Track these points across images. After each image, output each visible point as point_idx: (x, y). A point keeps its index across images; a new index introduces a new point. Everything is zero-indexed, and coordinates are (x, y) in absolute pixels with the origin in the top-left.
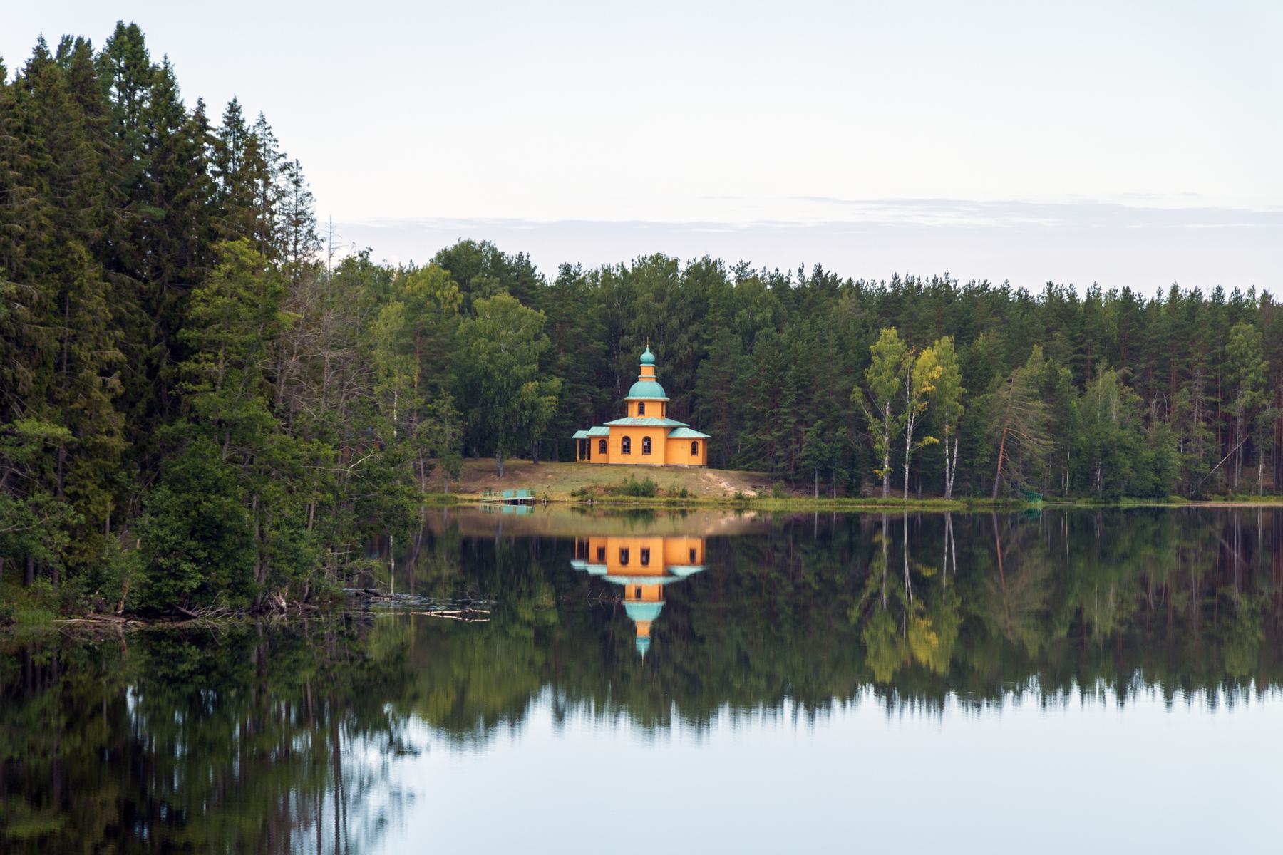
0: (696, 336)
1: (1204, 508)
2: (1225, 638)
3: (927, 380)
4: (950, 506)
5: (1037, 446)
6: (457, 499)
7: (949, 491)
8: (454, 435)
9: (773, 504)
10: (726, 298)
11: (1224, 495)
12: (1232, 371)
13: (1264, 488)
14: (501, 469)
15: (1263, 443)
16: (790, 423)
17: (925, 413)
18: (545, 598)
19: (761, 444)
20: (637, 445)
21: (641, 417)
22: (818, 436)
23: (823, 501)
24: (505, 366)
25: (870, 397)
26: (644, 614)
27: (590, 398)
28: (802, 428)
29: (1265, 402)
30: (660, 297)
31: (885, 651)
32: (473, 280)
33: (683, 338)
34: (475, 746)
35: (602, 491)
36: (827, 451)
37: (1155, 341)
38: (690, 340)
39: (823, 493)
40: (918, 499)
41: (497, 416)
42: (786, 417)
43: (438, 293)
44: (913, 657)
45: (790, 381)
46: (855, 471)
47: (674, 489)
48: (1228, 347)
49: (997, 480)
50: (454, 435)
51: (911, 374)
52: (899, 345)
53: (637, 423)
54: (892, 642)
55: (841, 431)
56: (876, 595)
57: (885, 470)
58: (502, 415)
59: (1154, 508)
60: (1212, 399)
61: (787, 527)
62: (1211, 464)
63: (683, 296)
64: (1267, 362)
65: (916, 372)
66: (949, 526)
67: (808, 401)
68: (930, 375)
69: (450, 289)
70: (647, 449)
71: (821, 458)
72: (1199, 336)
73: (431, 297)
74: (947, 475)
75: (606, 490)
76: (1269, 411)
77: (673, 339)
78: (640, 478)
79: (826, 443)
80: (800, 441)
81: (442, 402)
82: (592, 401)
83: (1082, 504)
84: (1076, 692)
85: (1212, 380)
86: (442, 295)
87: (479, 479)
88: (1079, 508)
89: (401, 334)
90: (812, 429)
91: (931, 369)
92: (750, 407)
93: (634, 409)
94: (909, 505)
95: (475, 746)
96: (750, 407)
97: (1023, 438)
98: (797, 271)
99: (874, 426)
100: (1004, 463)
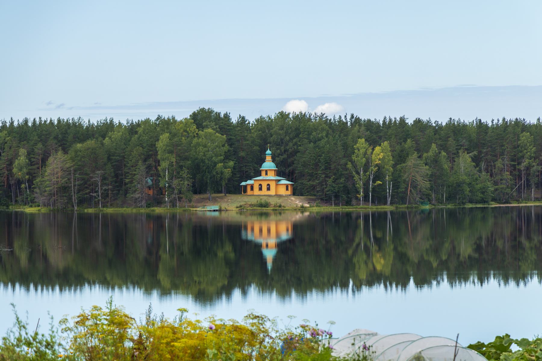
0: (296, 144)
1: (508, 207)
2: (521, 258)
3: (377, 159)
4: (388, 208)
5: (424, 184)
6: (190, 210)
7: (389, 203)
8: (188, 185)
9: (315, 209)
10: (307, 128)
11: (518, 201)
12: (521, 152)
13: (535, 198)
14: (211, 198)
15: (534, 180)
16: (322, 177)
17: (377, 172)
18: (228, 247)
19: (313, 186)
20: (264, 187)
21: (266, 176)
22: (333, 182)
23: (336, 208)
24: (210, 157)
25: (355, 166)
26: (269, 254)
27: (253, 169)
28: (327, 179)
29: (534, 164)
30: (282, 128)
31: (363, 266)
32: (204, 124)
33: (291, 144)
34: (211, 305)
35: (249, 206)
36: (336, 188)
37: (490, 140)
38: (294, 145)
39: (336, 204)
40: (375, 206)
41: (207, 177)
42: (320, 175)
43: (188, 129)
44: (374, 268)
45: (322, 161)
46: (349, 195)
47: (277, 204)
48: (519, 142)
49: (408, 198)
50: (188, 185)
51: (371, 156)
52: (366, 145)
53: (264, 179)
54: (366, 263)
55: (342, 180)
56: (359, 245)
57: (361, 195)
58: (209, 177)
59: (482, 207)
60: (513, 163)
61: (322, 218)
62: (511, 189)
63: (291, 128)
64: (535, 148)
65: (373, 156)
66: (389, 216)
67: (330, 168)
68: (378, 157)
69: (193, 128)
70: (269, 189)
71: (334, 191)
72: (508, 138)
73: (185, 131)
74: (388, 196)
75: (250, 205)
76: (535, 168)
77: (287, 145)
78: (264, 200)
79: (336, 185)
80: (326, 185)
81: (183, 172)
82: (254, 170)
83: (449, 206)
84: (57, 288)
85: (512, 156)
86: (190, 130)
87: (202, 202)
88: (449, 208)
89: (167, 146)
90: (331, 179)
91: (379, 155)
92: (307, 172)
93: (263, 173)
94: (371, 208)
95: (211, 305)
96: (307, 172)
97: (418, 181)
98: (344, 116)
99: (356, 177)
100: (411, 191)
